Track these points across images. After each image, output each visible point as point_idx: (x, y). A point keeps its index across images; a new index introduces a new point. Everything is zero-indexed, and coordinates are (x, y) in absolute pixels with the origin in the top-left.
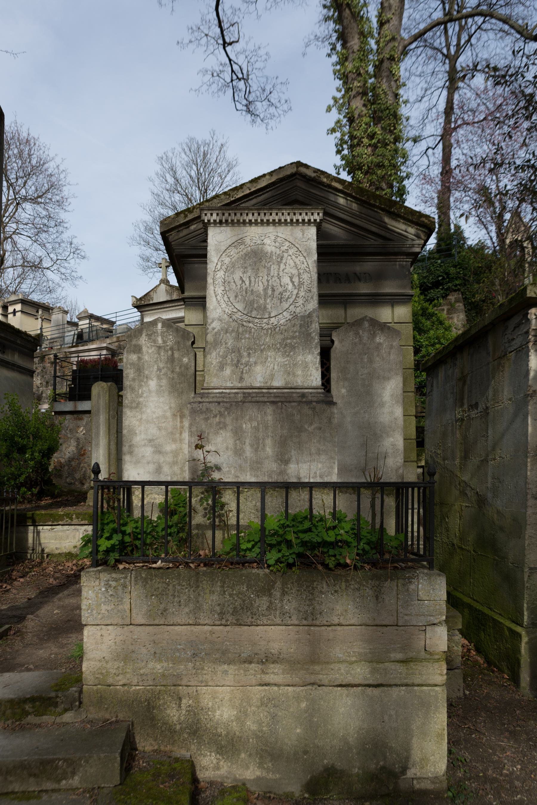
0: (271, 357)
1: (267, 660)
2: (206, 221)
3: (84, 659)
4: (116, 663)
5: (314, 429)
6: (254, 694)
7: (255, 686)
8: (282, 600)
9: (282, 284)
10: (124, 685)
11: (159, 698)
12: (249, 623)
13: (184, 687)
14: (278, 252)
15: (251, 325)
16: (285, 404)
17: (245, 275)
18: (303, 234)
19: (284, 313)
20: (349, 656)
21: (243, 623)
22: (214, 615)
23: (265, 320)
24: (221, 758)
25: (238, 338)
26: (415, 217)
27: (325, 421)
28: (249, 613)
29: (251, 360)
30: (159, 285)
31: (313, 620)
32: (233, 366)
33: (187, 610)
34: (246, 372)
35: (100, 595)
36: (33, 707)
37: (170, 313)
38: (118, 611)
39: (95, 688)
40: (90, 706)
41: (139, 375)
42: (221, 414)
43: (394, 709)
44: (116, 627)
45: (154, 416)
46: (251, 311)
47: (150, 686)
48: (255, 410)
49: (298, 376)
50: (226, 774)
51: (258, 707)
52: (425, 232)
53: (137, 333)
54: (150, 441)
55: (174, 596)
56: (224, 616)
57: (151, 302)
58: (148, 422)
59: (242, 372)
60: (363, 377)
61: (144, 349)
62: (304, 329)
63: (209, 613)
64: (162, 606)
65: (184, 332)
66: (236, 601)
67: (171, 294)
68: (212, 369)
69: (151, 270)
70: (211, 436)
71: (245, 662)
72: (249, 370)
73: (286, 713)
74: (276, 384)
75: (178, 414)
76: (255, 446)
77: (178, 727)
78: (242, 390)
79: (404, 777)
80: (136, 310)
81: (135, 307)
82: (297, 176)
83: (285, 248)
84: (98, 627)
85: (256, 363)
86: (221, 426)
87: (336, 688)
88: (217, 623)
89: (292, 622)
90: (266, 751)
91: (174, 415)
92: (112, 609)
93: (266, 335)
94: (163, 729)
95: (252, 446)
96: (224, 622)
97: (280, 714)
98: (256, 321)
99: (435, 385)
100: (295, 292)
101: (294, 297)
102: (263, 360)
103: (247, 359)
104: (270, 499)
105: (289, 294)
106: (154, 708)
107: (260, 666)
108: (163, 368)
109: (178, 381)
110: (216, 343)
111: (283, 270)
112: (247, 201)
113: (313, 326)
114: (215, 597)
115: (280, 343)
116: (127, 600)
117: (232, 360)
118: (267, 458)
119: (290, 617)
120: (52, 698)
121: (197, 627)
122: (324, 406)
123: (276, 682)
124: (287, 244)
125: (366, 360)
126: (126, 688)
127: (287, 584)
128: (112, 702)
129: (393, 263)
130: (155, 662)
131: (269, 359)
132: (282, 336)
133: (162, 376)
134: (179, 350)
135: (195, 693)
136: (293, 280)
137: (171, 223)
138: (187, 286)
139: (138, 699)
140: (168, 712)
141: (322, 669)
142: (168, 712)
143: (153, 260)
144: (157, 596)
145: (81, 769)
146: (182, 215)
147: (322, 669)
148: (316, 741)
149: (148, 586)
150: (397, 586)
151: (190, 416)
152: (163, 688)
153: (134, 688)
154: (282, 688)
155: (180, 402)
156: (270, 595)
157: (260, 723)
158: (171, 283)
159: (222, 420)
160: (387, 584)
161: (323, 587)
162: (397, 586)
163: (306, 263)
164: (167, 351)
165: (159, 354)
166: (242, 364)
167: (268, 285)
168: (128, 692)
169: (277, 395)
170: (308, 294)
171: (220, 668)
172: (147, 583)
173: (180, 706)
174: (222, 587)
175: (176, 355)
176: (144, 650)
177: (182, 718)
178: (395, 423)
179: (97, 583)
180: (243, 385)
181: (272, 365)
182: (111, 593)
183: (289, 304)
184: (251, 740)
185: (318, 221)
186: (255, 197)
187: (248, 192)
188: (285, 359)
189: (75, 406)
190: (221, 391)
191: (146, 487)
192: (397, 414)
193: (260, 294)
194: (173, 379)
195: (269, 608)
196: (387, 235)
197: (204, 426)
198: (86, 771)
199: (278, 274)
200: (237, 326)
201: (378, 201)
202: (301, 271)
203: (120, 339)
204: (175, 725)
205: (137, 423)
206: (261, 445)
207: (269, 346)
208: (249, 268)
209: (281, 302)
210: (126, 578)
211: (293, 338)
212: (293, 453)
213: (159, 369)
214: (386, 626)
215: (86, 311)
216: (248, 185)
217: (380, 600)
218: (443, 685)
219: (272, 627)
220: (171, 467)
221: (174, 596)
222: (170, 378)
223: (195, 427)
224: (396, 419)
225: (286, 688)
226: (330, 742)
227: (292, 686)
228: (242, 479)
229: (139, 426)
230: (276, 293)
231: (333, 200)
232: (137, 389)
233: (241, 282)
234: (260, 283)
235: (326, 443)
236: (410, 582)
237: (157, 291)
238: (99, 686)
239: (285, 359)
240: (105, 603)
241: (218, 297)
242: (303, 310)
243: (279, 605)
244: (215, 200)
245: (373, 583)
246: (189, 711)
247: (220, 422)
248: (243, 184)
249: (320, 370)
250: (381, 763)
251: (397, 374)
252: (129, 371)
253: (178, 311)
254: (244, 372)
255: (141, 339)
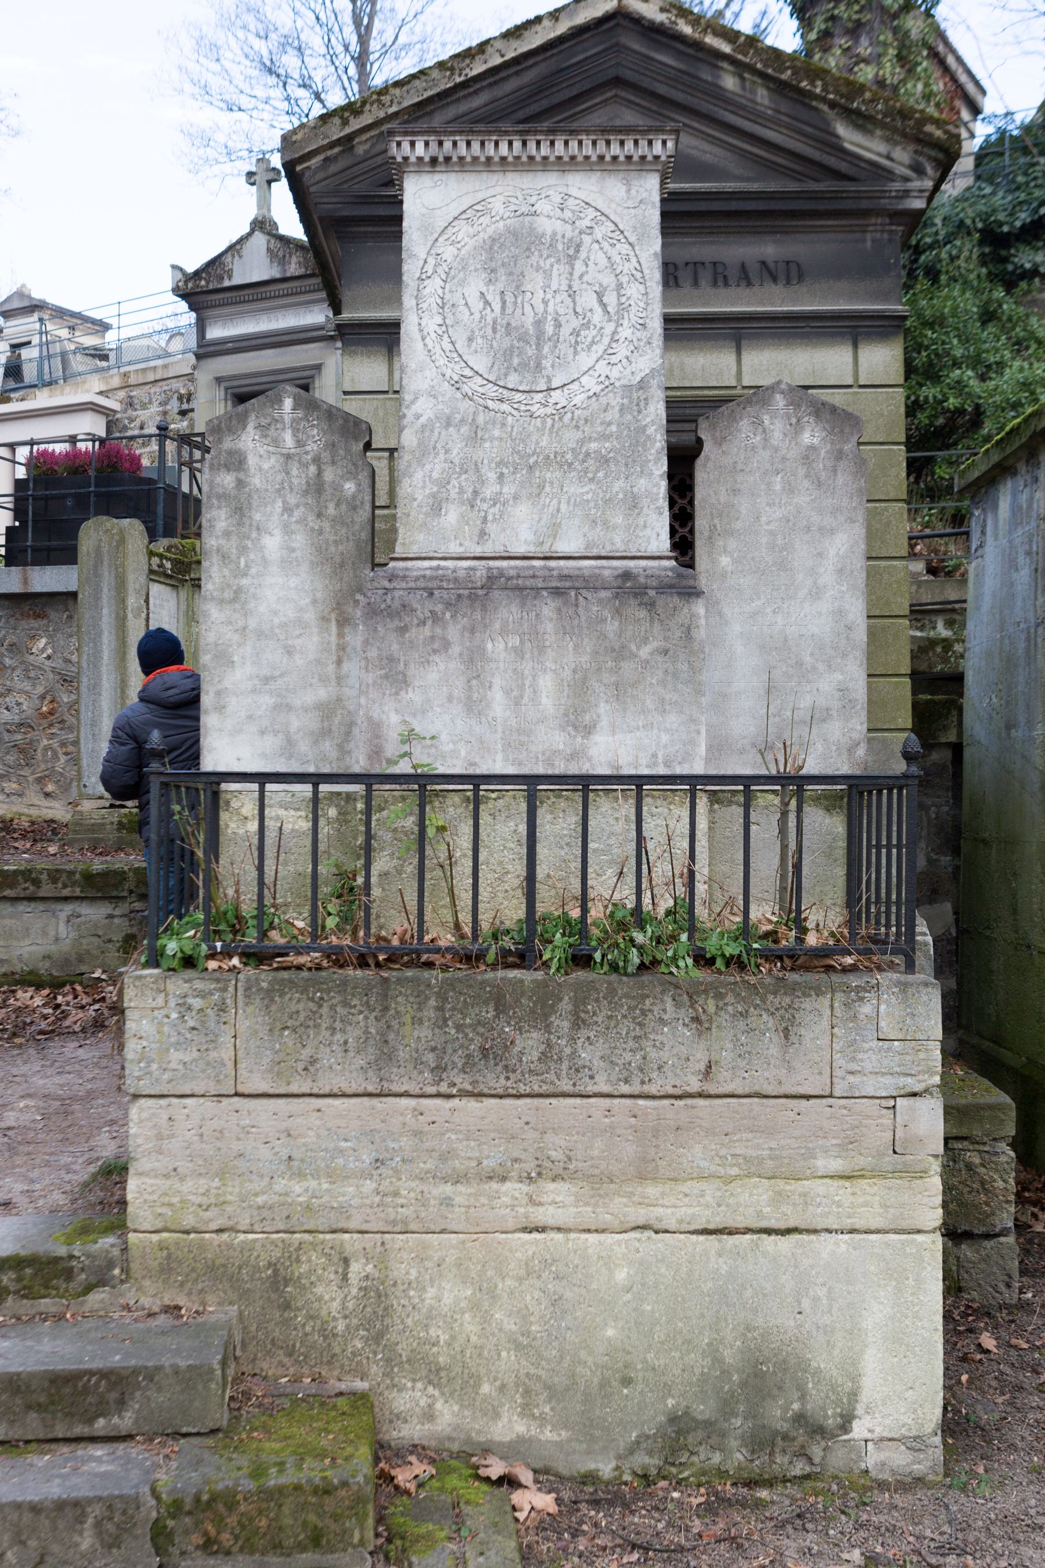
0: (551, 483)
1: (539, 1174)
2: (399, 159)
3: (131, 1171)
4: (202, 1181)
5: (651, 654)
6: (511, 1251)
7: (514, 1232)
8: (573, 1040)
9: (579, 310)
10: (220, 1231)
11: (298, 1260)
12: (500, 1091)
13: (355, 1236)
14: (569, 234)
15: (505, 407)
16: (584, 592)
17: (492, 288)
18: (628, 191)
19: (584, 380)
20: (723, 1165)
21: (486, 1091)
22: (421, 1072)
23: (539, 397)
24: (437, 1393)
25: (475, 438)
26: (911, 123)
27: (678, 634)
28: (499, 1068)
29: (505, 490)
30: (249, 235)
31: (643, 1082)
32: (463, 503)
33: (360, 1062)
34: (494, 520)
35: (166, 1029)
36: (19, 1280)
37: (279, 314)
38: (208, 1064)
39: (155, 1237)
40: (144, 1277)
41: (240, 524)
42: (435, 618)
43: (824, 1285)
44: (202, 1100)
45: (276, 621)
46: (506, 375)
47: (278, 1232)
48: (514, 610)
49: (615, 528)
50: (449, 1429)
51: (520, 1280)
52: (935, 160)
53: (234, 422)
54: (267, 680)
55: (333, 1030)
56: (444, 1076)
57: (227, 283)
58: (260, 634)
59: (485, 518)
60: (772, 527)
61: (252, 461)
62: (629, 417)
63: (410, 1067)
64: (306, 1053)
65: (346, 421)
66: (472, 1040)
67: (283, 262)
68: (413, 513)
69: (216, 169)
70: (412, 671)
71: (491, 1178)
72: (502, 514)
73: (583, 1291)
74: (563, 547)
75: (333, 616)
76: (515, 693)
77: (341, 1326)
78: (483, 562)
79: (845, 1437)
80: (183, 306)
81: (184, 296)
82: (622, 22)
83: (587, 222)
84: (163, 1102)
85: (516, 497)
86: (436, 646)
87: (694, 1237)
88: (431, 1090)
89: (596, 1089)
90: (539, 1378)
91: (325, 619)
92: (194, 1060)
93: (541, 430)
94: (308, 1329)
95: (507, 692)
96: (444, 1088)
97: (568, 1294)
98: (518, 397)
99: (989, 529)
100: (610, 328)
101: (606, 340)
102: (535, 490)
103: (496, 488)
104: (549, 817)
105: (594, 332)
106: (287, 1282)
107: (525, 1188)
108: (297, 506)
109: (332, 538)
110: (424, 451)
111: (581, 277)
112: (496, 83)
113: (651, 408)
114: (425, 1032)
115: (573, 450)
116: (226, 1039)
117: (462, 491)
118: (542, 721)
119: (592, 1077)
120: (61, 1258)
121: (384, 1099)
122: (676, 599)
123: (560, 1223)
124: (591, 213)
125: (778, 487)
126: (225, 1236)
127: (584, 1004)
128: (193, 1270)
129: (858, 235)
130: (290, 1179)
131: (548, 489)
132: (579, 435)
133: (294, 527)
134: (334, 463)
135: (379, 1249)
136: (605, 300)
137: (306, 140)
138: (347, 295)
139: (253, 1262)
140: (319, 1290)
141: (663, 1194)
142: (319, 1290)
143: (221, 138)
144: (294, 1031)
145: (138, 1394)
146: (337, 121)
147: (663, 1194)
148: (650, 1356)
149: (274, 1008)
150: (832, 1007)
151: (365, 624)
152: (306, 1236)
153: (242, 1237)
154: (572, 1235)
155: (338, 587)
156: (548, 1028)
157: (524, 1315)
158: (283, 231)
159: (439, 631)
160: (807, 1004)
161: (664, 1010)
162: (832, 1007)
163: (634, 260)
164: (306, 466)
165: (288, 473)
166: (483, 500)
167: (546, 312)
168: (230, 1246)
169: (566, 572)
170: (638, 334)
171: (436, 1192)
172: (272, 1000)
173: (345, 1278)
174: (440, 1009)
175: (329, 475)
176: (265, 1152)
177: (350, 1305)
178: (848, 638)
179: (160, 1000)
180: (488, 549)
181: (555, 501)
182: (191, 1023)
183: (594, 356)
184: (504, 1354)
185: (663, 158)
186: (517, 73)
187: (497, 61)
188: (586, 489)
189: (25, 581)
190: (434, 563)
191: (269, 787)
192: (851, 617)
193: (526, 333)
194: (321, 532)
195: (544, 1057)
196: (843, 167)
197: (395, 647)
198: (149, 1399)
199: (570, 287)
200: (472, 410)
201: (819, 83)
202: (624, 279)
203: (132, 380)
204: (335, 1319)
205: (236, 637)
206: (528, 692)
207: (548, 457)
208: (501, 271)
209: (576, 353)
210: (225, 990)
211: (605, 437)
212: (603, 708)
213: (287, 510)
214: (808, 1097)
215: (20, 294)
216: (498, 45)
217: (793, 1038)
218: (934, 1231)
219: (553, 1101)
220: (316, 742)
221: (333, 1030)
222: (312, 529)
223: (375, 649)
224: (849, 628)
225: (585, 1236)
226: (682, 1358)
227: (596, 1231)
228: (483, 769)
229: (239, 645)
230: (565, 331)
231: (710, 79)
232: (234, 557)
233: (481, 305)
234: (528, 308)
235: (680, 686)
236: (862, 999)
237: (244, 252)
238: (165, 1235)
239: (586, 489)
240: (177, 1045)
241: (428, 340)
242: (628, 371)
243: (568, 1051)
244: (417, 82)
245: (777, 1001)
246: (366, 1288)
247: (432, 638)
248: (487, 42)
249: (667, 513)
250: (796, 1406)
251: (853, 521)
252: (214, 513)
253: (302, 310)
254: (490, 518)
255: (244, 437)
